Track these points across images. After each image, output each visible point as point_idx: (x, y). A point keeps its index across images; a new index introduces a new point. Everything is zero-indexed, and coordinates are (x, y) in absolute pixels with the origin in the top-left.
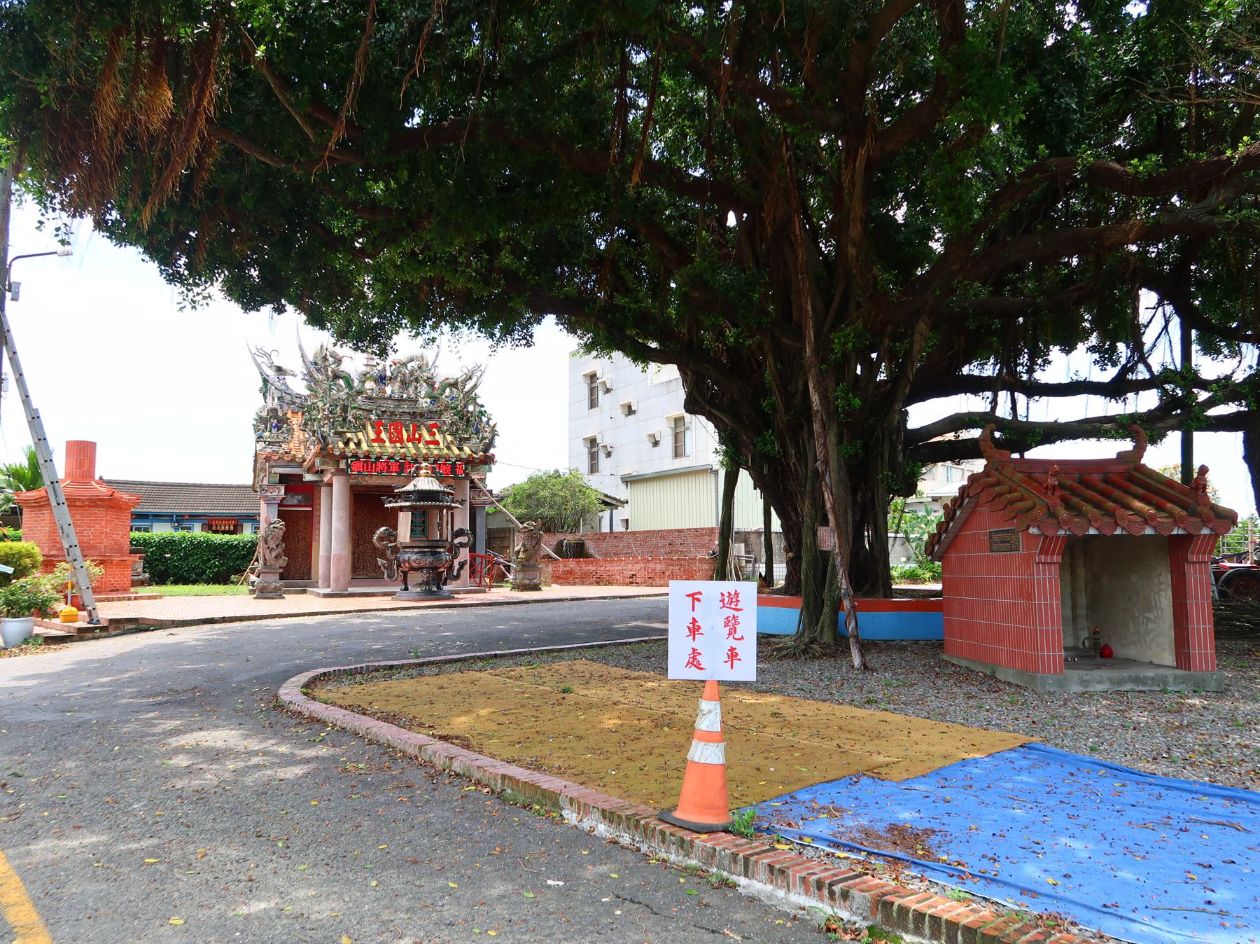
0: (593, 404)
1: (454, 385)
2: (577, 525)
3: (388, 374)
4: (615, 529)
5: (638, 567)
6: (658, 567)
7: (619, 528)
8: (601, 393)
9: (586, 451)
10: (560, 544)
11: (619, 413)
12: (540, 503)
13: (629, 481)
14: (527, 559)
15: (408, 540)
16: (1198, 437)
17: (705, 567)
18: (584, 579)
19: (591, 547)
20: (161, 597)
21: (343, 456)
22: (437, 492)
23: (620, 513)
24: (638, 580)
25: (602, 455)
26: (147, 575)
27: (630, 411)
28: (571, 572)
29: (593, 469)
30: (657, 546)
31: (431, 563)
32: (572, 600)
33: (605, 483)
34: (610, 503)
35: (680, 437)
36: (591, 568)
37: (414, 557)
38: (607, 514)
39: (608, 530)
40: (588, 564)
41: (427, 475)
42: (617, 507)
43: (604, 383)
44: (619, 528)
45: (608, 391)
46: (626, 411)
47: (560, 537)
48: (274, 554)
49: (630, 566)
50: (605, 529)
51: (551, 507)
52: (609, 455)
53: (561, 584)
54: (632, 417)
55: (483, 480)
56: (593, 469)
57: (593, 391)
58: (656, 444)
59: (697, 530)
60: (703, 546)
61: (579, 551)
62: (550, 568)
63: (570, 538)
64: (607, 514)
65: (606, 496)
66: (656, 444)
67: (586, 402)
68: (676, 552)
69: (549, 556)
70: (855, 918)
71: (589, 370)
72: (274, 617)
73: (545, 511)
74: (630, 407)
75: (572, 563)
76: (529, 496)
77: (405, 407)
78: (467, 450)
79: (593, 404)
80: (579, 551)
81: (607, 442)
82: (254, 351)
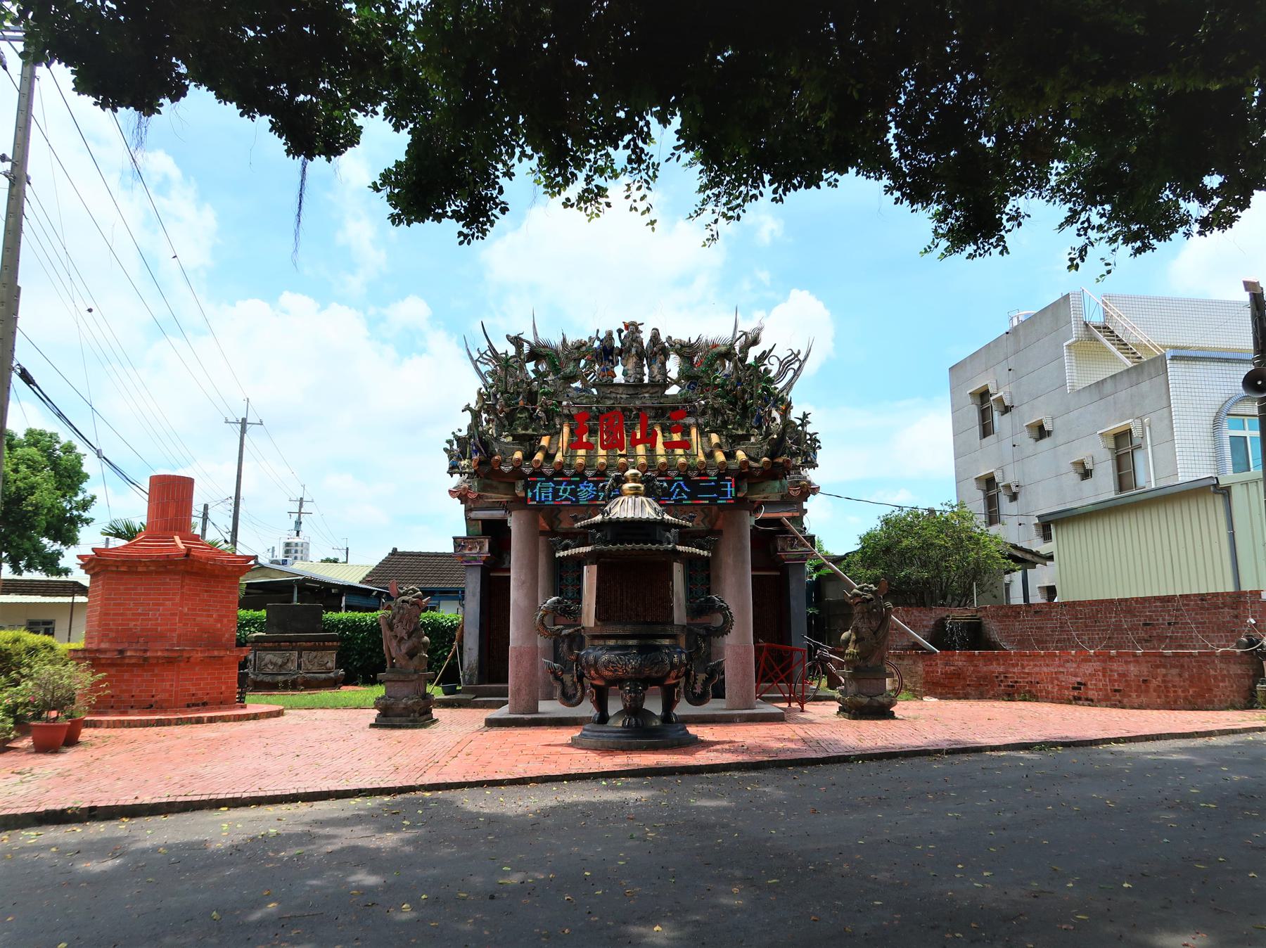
0: (986, 430)
1: (727, 354)
2: (967, 594)
3: (617, 344)
4: (1032, 601)
5: (1088, 668)
6: (1133, 669)
7: (1037, 598)
8: (996, 414)
9: (980, 494)
10: (941, 623)
11: (1026, 438)
12: (906, 557)
13: (1046, 526)
14: (863, 656)
15: (592, 625)
16: (1230, 588)
17: (1236, 669)
18: (983, 689)
19: (994, 629)
20: (279, 714)
21: (517, 473)
22: (647, 523)
23: (1041, 576)
24: (1091, 694)
25: (1004, 500)
26: (341, 672)
27: (1041, 432)
28: (958, 675)
29: (993, 517)
30: (1118, 628)
31: (637, 670)
32: (952, 752)
33: (1015, 529)
34: (1024, 559)
35: (1124, 460)
36: (996, 668)
37: (605, 657)
38: (1017, 577)
39: (1021, 602)
40: (988, 661)
41: (636, 492)
42: (1033, 565)
43: (1000, 400)
44: (1037, 598)
45: (1006, 410)
46: (1036, 434)
47: (939, 613)
48: (404, 648)
49: (1071, 667)
50: (1017, 598)
51: (924, 565)
52: (1014, 497)
53: (942, 697)
54: (1045, 442)
55: (798, 521)
56: (993, 517)
57: (985, 415)
58: (1086, 474)
59: (1202, 597)
60: (1221, 627)
61: (975, 637)
62: (920, 668)
63: (956, 615)
64: (1017, 577)
65: (1015, 547)
66: (1086, 474)
67: (977, 430)
68: (1161, 639)
69: (916, 646)
70: (1037, 669)
71: (977, 386)
72: (215, 804)
73: (913, 572)
74: (1041, 428)
75: (959, 659)
76: (887, 550)
77: (646, 399)
78: (741, 455)
79: (986, 430)
80: (975, 637)
81: (1011, 478)
82: (476, 356)
